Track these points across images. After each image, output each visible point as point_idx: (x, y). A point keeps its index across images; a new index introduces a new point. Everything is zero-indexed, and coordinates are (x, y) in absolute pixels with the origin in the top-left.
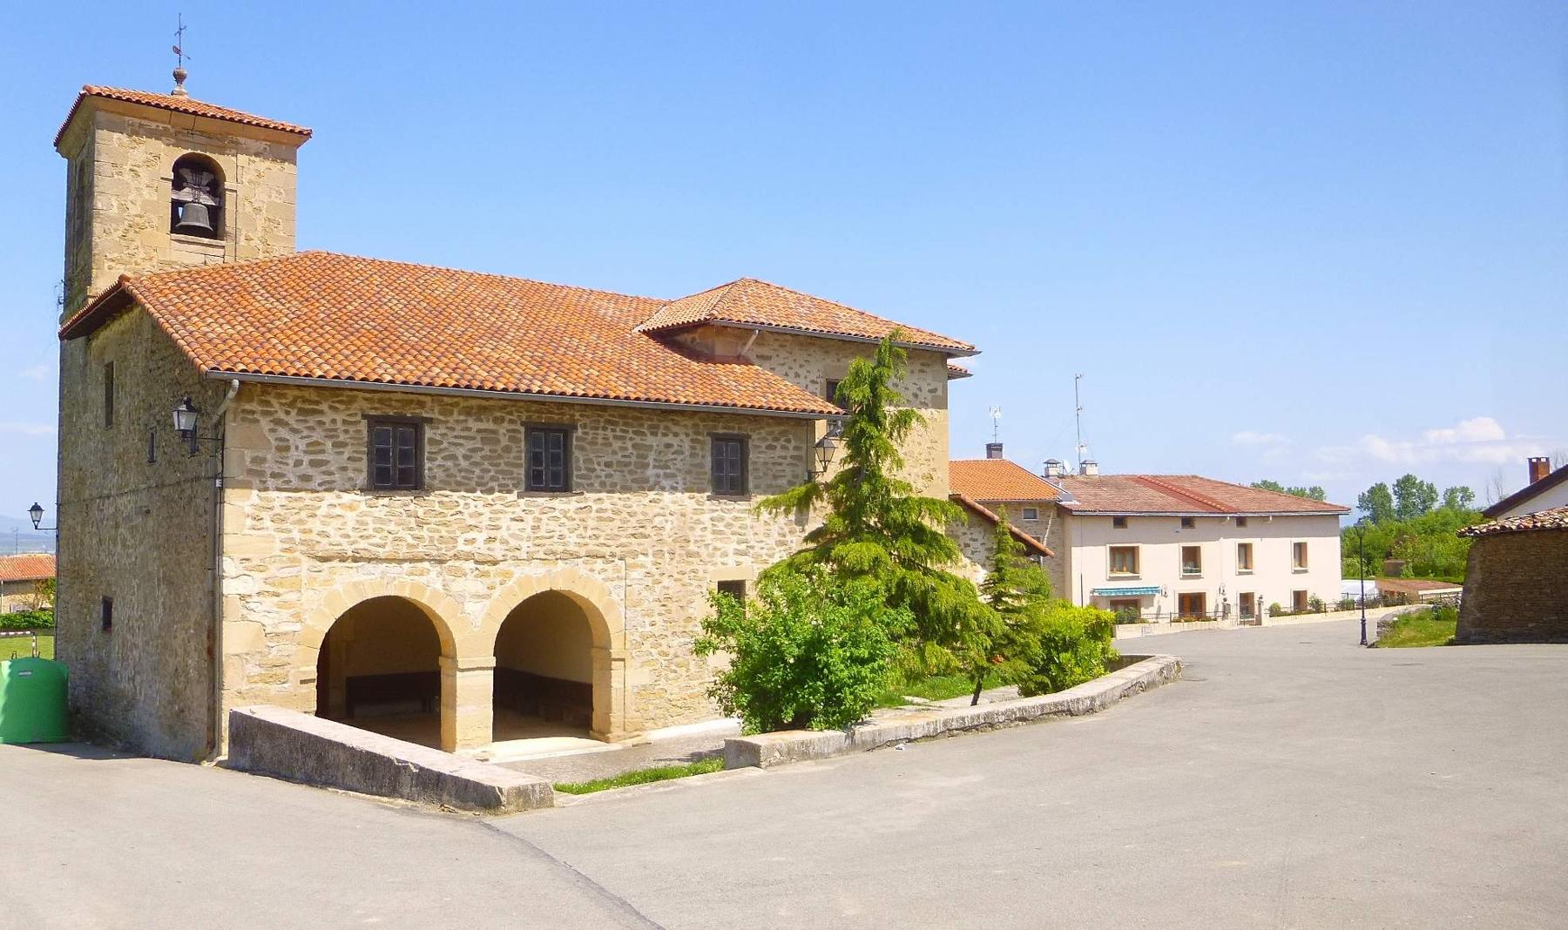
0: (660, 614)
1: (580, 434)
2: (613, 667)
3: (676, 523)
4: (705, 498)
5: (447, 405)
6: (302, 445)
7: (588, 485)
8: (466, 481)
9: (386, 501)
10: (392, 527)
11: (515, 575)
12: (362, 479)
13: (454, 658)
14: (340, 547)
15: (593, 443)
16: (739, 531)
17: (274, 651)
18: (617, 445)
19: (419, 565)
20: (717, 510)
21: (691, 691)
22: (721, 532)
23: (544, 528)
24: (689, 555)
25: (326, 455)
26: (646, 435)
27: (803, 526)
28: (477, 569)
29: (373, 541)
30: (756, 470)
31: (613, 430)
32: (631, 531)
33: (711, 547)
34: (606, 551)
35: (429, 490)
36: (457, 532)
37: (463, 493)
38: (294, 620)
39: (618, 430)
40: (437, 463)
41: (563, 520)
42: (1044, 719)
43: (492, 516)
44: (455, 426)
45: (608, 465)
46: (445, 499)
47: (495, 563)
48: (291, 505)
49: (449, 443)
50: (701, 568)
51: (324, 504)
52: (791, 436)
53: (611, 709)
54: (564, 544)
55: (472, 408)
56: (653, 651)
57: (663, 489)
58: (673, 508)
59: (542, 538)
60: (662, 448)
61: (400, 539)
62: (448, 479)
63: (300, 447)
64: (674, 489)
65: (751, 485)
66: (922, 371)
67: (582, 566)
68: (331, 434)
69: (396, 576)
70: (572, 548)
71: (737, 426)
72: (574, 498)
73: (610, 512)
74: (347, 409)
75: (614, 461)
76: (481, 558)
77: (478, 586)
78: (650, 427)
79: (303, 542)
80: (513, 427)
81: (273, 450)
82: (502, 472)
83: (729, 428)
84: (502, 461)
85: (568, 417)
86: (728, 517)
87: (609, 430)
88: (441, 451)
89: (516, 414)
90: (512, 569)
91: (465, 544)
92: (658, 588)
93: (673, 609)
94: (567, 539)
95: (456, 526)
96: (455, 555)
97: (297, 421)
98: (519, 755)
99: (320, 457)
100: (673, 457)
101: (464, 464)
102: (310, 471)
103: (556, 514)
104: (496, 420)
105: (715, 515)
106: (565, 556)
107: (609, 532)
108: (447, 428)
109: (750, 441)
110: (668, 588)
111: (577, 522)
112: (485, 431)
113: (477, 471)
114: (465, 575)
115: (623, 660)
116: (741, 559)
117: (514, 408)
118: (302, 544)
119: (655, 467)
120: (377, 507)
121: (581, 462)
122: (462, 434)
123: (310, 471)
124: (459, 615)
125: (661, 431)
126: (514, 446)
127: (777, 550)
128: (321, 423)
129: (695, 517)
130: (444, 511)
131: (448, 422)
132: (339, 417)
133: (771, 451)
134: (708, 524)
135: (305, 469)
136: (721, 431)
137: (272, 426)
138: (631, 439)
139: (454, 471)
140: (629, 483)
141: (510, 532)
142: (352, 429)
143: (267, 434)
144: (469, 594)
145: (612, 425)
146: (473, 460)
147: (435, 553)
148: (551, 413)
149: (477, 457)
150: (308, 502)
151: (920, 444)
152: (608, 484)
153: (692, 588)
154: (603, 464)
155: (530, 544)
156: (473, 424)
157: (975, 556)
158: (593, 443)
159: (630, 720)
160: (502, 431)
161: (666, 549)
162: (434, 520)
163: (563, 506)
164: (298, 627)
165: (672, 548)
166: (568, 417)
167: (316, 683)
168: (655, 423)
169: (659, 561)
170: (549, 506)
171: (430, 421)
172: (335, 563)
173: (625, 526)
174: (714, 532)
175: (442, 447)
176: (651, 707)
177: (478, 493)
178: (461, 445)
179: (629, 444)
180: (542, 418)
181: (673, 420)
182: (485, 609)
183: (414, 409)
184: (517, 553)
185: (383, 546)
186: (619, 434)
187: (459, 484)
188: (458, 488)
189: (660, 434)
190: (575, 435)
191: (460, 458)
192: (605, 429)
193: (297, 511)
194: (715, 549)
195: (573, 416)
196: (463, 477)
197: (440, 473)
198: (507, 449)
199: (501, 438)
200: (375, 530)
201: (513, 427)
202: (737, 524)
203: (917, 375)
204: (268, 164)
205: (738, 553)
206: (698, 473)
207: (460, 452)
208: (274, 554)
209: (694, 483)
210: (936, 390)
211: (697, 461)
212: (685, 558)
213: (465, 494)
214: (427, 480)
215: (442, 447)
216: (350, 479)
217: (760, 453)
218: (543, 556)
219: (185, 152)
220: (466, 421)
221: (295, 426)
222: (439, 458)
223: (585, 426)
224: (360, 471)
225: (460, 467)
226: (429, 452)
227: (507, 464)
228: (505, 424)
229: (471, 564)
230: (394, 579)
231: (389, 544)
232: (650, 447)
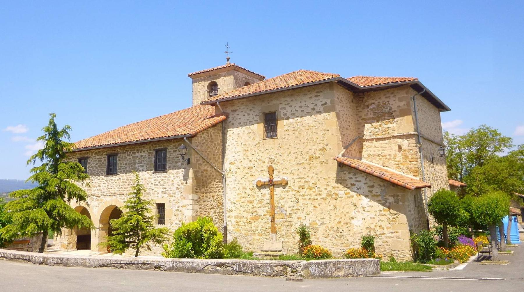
15: (122, 158)
16: (163, 184)
18: (128, 157)
22: (157, 185)
23: (110, 186)
27: (186, 181)
31: (127, 153)
33: (154, 191)
34: (124, 192)
37: (94, 177)
41: (114, 183)
42: (15, 260)
45: (126, 164)
47: (100, 197)
57: (140, 171)
60: (140, 157)
65: (167, 167)
66: (316, 96)
70: (116, 192)
72: (117, 176)
83: (160, 147)
86: (159, 179)
100: (144, 159)
106: (114, 194)
107: (125, 186)
109: (167, 150)
111: (118, 183)
116: (163, 195)
119: (138, 164)
129: (149, 180)
133: (175, 153)
134: (153, 182)
136: (157, 148)
138: (132, 155)
151: (317, 133)
157: (360, 191)
158: (122, 158)
160: (102, 158)
174: (155, 185)
177: (97, 177)
178: (94, 163)
179: (131, 157)
186: (129, 154)
187: (93, 174)
194: (155, 191)
198: (103, 163)
202: (162, 182)
203: (314, 98)
204: (227, 78)
205: (163, 193)
209: (149, 168)
210: (326, 103)
211: (150, 160)
217: (171, 154)
218: (110, 195)
219: (209, 82)
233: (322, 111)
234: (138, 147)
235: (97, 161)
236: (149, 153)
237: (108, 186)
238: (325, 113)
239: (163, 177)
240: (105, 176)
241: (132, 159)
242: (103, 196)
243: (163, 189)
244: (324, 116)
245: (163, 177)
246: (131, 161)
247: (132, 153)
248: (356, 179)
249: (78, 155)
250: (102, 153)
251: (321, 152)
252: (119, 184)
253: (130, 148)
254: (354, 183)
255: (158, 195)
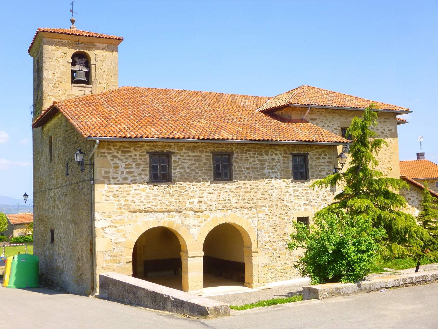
15: (241, 159)
16: (305, 195)
18: (251, 160)
23: (222, 196)
27: (334, 192)
31: (249, 154)
33: (293, 203)
34: (248, 205)
41: (230, 193)
45: (248, 168)
47: (202, 212)
57: (272, 178)
60: (270, 160)
66: (385, 122)
70: (234, 205)
72: (234, 183)
86: (300, 189)
107: (249, 197)
109: (309, 156)
119: (268, 169)
129: (286, 190)
134: (292, 192)
136: (296, 152)
138: (257, 157)
151: (385, 154)
157: (413, 204)
158: (241, 159)
160: (203, 156)
177: (194, 183)
178: (186, 163)
179: (256, 159)
186: (252, 155)
194: (295, 203)
202: (304, 192)
204: (107, 53)
205: (305, 205)
209: (285, 175)
211: (286, 165)
218: (222, 209)
219: (78, 50)
233: (389, 136)
234: (267, 147)
235: (192, 160)
236: (283, 157)
237: (219, 196)
238: (391, 138)
239: (305, 187)
240: (211, 183)
241: (257, 162)
242: (208, 211)
243: (306, 200)
244: (390, 140)
245: (305, 187)
246: (256, 165)
247: (258, 154)
248: (411, 195)
249: (148, 148)
250: (201, 149)
251: (389, 171)
252: (238, 194)
253: (254, 148)
254: (410, 198)
255: (300, 208)
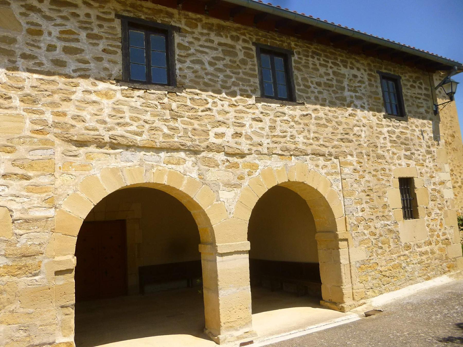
0: (367, 202)
1: (297, 59)
2: (340, 247)
3: (367, 133)
4: (383, 117)
5: (192, 19)
6: (55, 31)
7: (307, 98)
8: (212, 83)
9: (141, 92)
10: (148, 117)
11: (260, 167)
12: (117, 70)
13: (213, 244)
14: (97, 133)
15: (306, 66)
17: (23, 240)
18: (322, 70)
19: (176, 154)
20: (390, 126)
21: (393, 263)
23: (278, 128)
24: (379, 157)
25: (80, 43)
26: (340, 66)
28: (228, 161)
29: (129, 128)
30: (407, 100)
31: (319, 59)
32: (340, 136)
34: (325, 150)
35: (182, 87)
36: (208, 126)
37: (211, 93)
38: (47, 205)
39: (321, 59)
40: (186, 65)
41: (292, 123)
43: (237, 115)
44: (200, 37)
45: (319, 84)
46: (196, 97)
47: (242, 156)
48: (44, 87)
49: (195, 50)
50: (387, 167)
51: (79, 89)
52: (422, 81)
53: (342, 282)
54: (295, 143)
55: (213, 25)
56: (366, 232)
57: (356, 106)
58: (365, 121)
59: (278, 136)
60: (351, 77)
61: (156, 129)
62: (197, 80)
63: (54, 34)
64: (363, 108)
67: (309, 162)
68: (85, 25)
69: (154, 163)
70: (301, 146)
71: (392, 69)
73: (324, 120)
74: (101, 7)
75: (322, 82)
76: (230, 151)
77: (229, 176)
78: (342, 61)
79: (56, 125)
80: (246, 45)
81: (24, 32)
82: (241, 79)
84: (241, 71)
85: (286, 44)
87: (316, 59)
88: (188, 55)
89: (248, 36)
90: (257, 161)
91: (216, 138)
92: (363, 181)
93: (374, 198)
94: (297, 139)
95: (206, 121)
96: (208, 147)
97: (50, 9)
98: (278, 332)
99: (74, 45)
100: (359, 84)
101: (210, 69)
102: (64, 57)
103: (286, 118)
104: (232, 38)
105: (390, 129)
108: (193, 38)
110: (369, 182)
112: (225, 45)
113: (221, 76)
114: (218, 166)
115: (346, 240)
117: (246, 31)
118: (55, 127)
119: (349, 90)
120: (133, 97)
121: (300, 79)
122: (206, 44)
123: (64, 57)
124: (215, 202)
125: (349, 65)
126: (249, 60)
127: (427, 157)
128: (75, 15)
130: (195, 107)
131: (194, 33)
132: (93, 13)
134: (387, 135)
135: (58, 54)
136: (384, 71)
137: (23, 10)
138: (331, 68)
139: (201, 73)
140: (334, 100)
141: (253, 130)
142: (106, 24)
143: (18, 16)
144: (222, 183)
145: (317, 55)
146: (216, 66)
147: (189, 143)
148: (276, 39)
149: (220, 65)
150: (61, 86)
151: (446, 118)
152: (320, 99)
153: (384, 182)
154: (314, 83)
155: (269, 141)
156: (217, 40)
159: (358, 291)
160: (238, 47)
161: (364, 151)
162: (187, 114)
163: (291, 112)
164: (51, 212)
165: (368, 151)
166: (286, 44)
167: (74, 272)
168: (345, 59)
169: (361, 160)
170: (281, 110)
171: (179, 30)
172: (92, 148)
173: (335, 132)
175: (190, 52)
176: (370, 278)
177: (224, 95)
179: (330, 71)
180: (268, 42)
181: (354, 58)
182: (237, 197)
183: (163, 17)
184: (260, 148)
185: (140, 134)
186: (323, 62)
187: (206, 84)
188: (205, 88)
189: (348, 67)
190: (293, 58)
191: (207, 64)
192: (313, 57)
193: (50, 93)
194: (393, 153)
195: (289, 44)
196: (210, 80)
197: (190, 74)
198: (244, 62)
199: (239, 53)
200: (132, 118)
201: (246, 45)
202: (403, 136)
205: (406, 157)
206: (375, 98)
207: (206, 59)
208: (23, 134)
209: (374, 105)
211: (374, 89)
212: (376, 159)
213: (212, 94)
214: (179, 79)
215: (190, 52)
216: (106, 69)
218: (280, 152)
220: (208, 34)
221: (48, 14)
222: (188, 62)
223: (299, 53)
224: (115, 63)
225: (206, 71)
226: (178, 55)
227: (244, 73)
228: (240, 42)
229: (221, 157)
230: (153, 167)
231: (146, 133)
232: (344, 75)
